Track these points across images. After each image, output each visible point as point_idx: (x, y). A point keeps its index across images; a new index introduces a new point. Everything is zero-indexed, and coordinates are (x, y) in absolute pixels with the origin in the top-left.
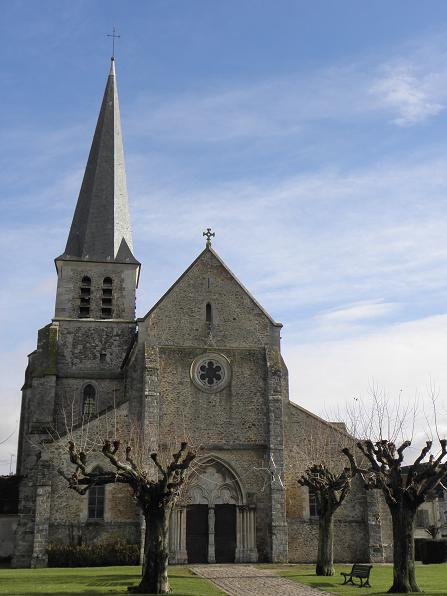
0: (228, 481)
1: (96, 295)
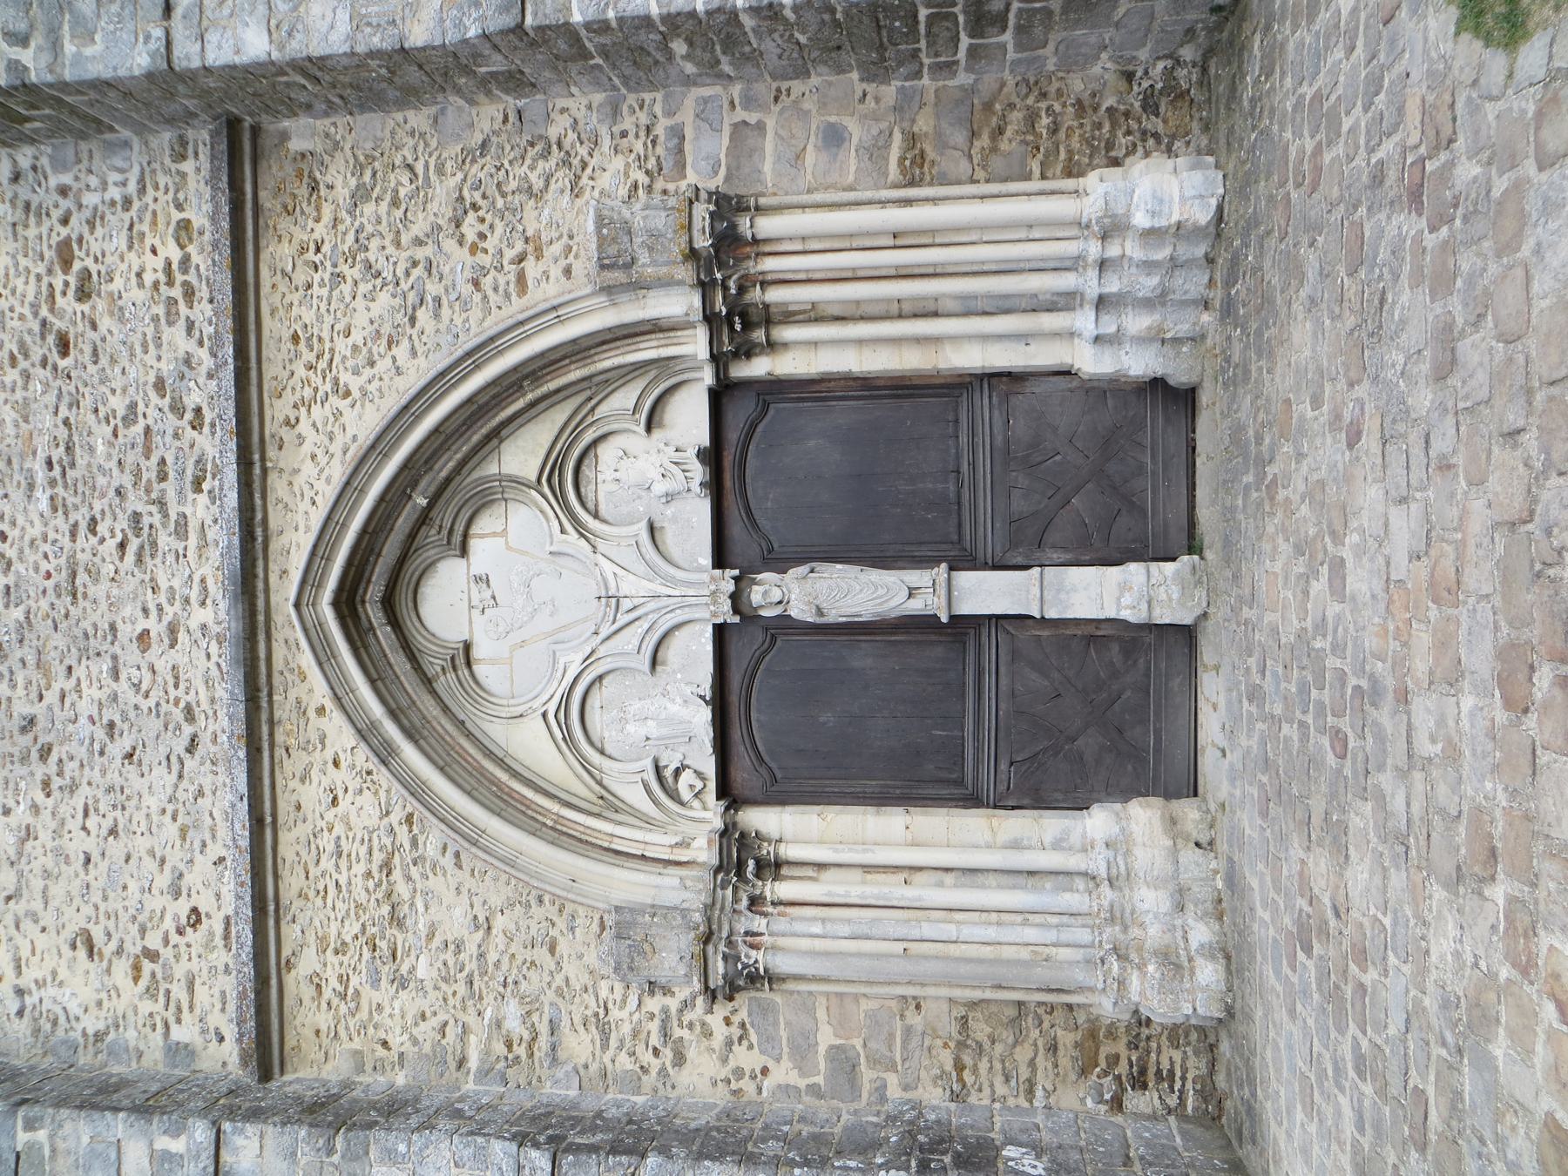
0: (522, 455)
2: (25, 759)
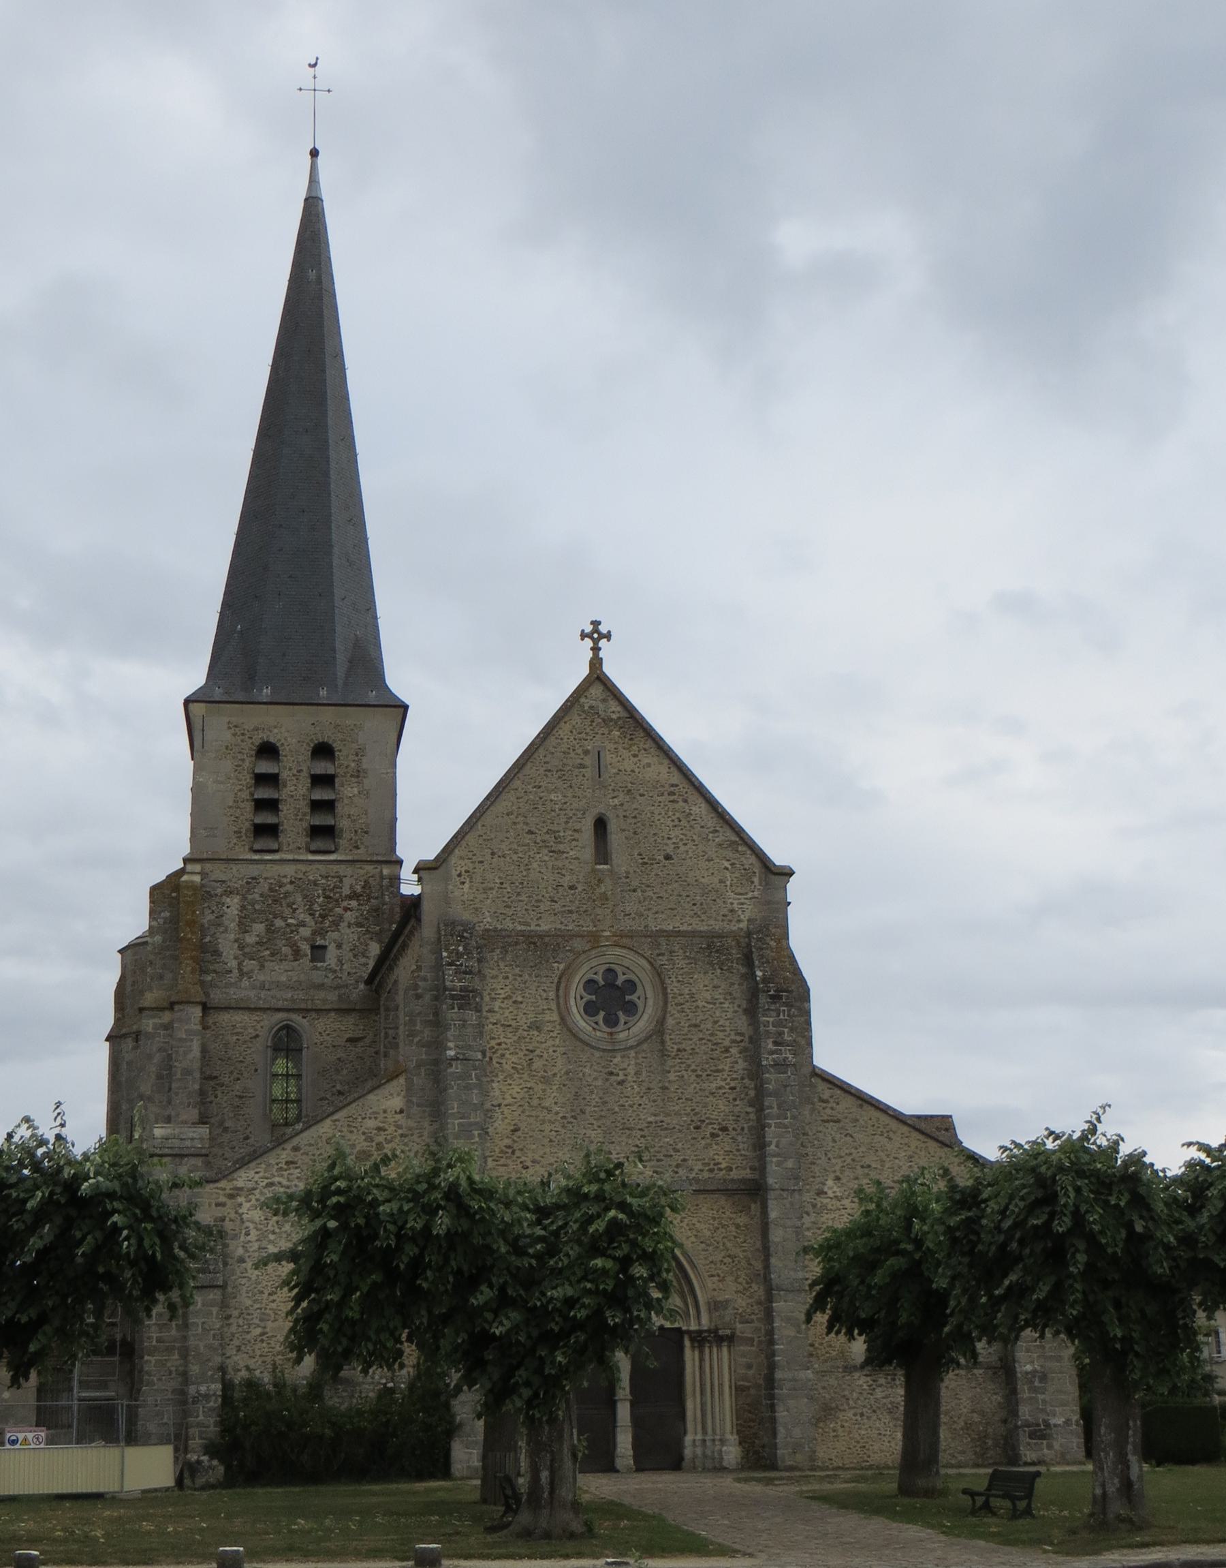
1: (295, 793)
2: (572, 1110)
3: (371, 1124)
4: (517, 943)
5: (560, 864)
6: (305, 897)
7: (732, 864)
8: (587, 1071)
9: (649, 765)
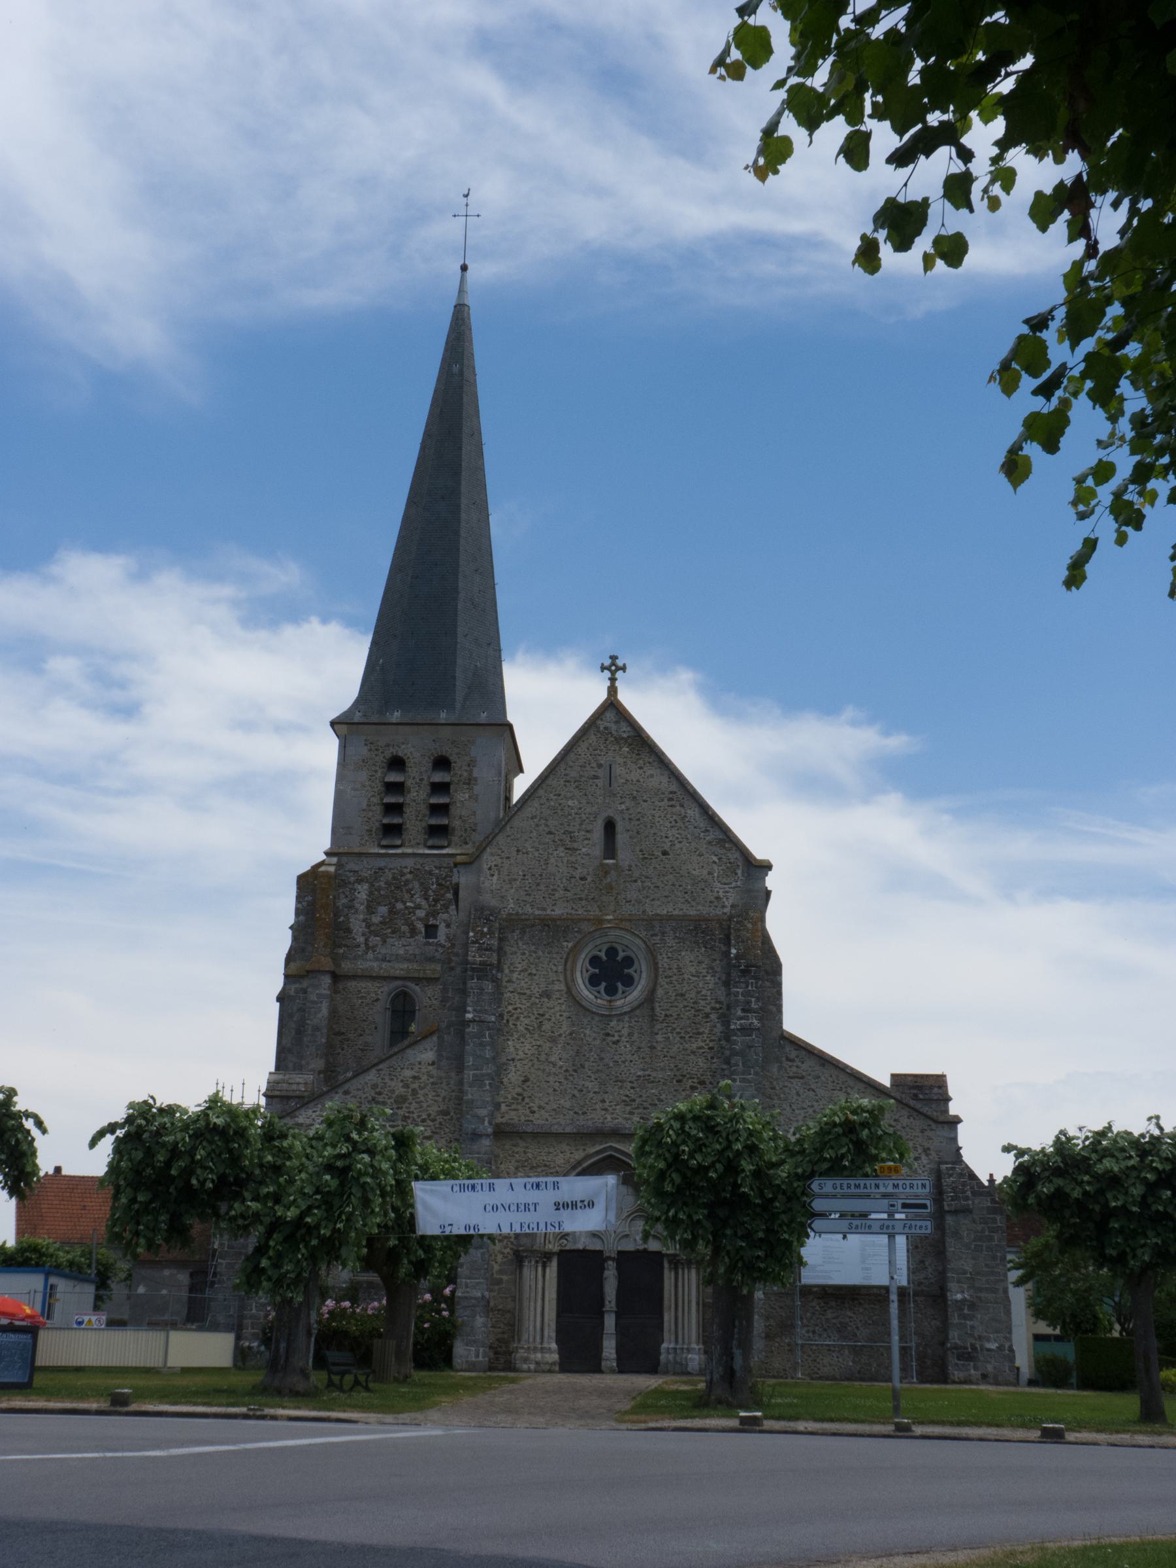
1: (417, 797)
3: (408, 1073)
4: (533, 926)
5: (573, 859)
6: (421, 884)
7: (720, 859)
8: (587, 1032)
9: (652, 776)
